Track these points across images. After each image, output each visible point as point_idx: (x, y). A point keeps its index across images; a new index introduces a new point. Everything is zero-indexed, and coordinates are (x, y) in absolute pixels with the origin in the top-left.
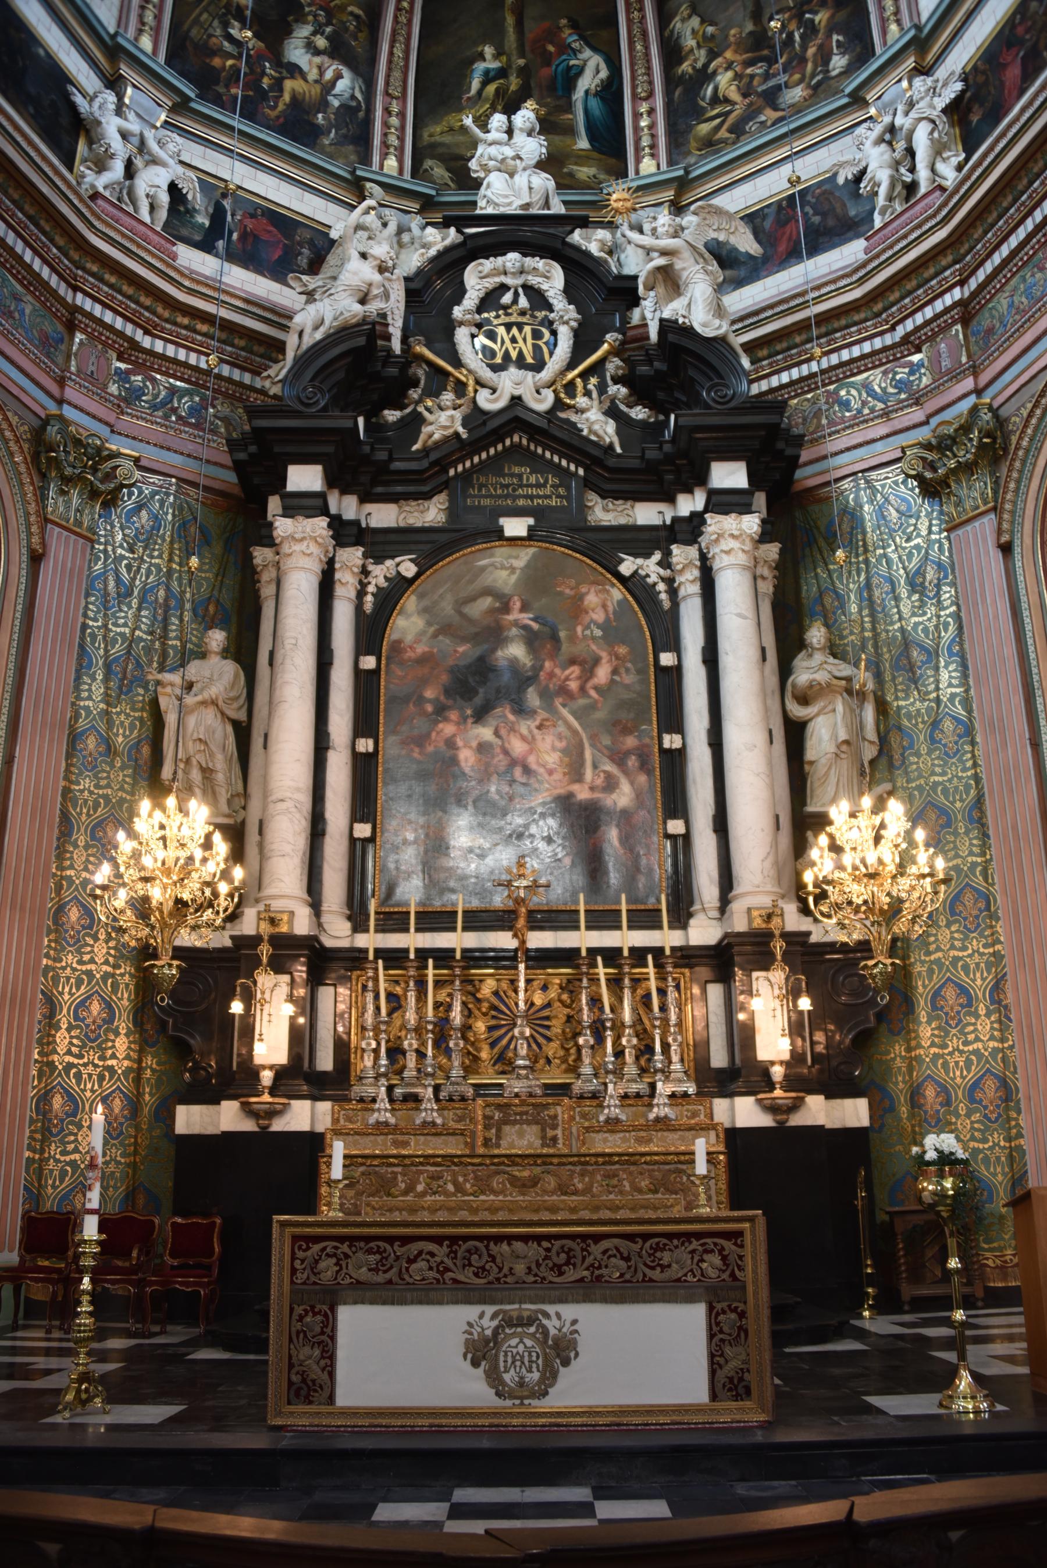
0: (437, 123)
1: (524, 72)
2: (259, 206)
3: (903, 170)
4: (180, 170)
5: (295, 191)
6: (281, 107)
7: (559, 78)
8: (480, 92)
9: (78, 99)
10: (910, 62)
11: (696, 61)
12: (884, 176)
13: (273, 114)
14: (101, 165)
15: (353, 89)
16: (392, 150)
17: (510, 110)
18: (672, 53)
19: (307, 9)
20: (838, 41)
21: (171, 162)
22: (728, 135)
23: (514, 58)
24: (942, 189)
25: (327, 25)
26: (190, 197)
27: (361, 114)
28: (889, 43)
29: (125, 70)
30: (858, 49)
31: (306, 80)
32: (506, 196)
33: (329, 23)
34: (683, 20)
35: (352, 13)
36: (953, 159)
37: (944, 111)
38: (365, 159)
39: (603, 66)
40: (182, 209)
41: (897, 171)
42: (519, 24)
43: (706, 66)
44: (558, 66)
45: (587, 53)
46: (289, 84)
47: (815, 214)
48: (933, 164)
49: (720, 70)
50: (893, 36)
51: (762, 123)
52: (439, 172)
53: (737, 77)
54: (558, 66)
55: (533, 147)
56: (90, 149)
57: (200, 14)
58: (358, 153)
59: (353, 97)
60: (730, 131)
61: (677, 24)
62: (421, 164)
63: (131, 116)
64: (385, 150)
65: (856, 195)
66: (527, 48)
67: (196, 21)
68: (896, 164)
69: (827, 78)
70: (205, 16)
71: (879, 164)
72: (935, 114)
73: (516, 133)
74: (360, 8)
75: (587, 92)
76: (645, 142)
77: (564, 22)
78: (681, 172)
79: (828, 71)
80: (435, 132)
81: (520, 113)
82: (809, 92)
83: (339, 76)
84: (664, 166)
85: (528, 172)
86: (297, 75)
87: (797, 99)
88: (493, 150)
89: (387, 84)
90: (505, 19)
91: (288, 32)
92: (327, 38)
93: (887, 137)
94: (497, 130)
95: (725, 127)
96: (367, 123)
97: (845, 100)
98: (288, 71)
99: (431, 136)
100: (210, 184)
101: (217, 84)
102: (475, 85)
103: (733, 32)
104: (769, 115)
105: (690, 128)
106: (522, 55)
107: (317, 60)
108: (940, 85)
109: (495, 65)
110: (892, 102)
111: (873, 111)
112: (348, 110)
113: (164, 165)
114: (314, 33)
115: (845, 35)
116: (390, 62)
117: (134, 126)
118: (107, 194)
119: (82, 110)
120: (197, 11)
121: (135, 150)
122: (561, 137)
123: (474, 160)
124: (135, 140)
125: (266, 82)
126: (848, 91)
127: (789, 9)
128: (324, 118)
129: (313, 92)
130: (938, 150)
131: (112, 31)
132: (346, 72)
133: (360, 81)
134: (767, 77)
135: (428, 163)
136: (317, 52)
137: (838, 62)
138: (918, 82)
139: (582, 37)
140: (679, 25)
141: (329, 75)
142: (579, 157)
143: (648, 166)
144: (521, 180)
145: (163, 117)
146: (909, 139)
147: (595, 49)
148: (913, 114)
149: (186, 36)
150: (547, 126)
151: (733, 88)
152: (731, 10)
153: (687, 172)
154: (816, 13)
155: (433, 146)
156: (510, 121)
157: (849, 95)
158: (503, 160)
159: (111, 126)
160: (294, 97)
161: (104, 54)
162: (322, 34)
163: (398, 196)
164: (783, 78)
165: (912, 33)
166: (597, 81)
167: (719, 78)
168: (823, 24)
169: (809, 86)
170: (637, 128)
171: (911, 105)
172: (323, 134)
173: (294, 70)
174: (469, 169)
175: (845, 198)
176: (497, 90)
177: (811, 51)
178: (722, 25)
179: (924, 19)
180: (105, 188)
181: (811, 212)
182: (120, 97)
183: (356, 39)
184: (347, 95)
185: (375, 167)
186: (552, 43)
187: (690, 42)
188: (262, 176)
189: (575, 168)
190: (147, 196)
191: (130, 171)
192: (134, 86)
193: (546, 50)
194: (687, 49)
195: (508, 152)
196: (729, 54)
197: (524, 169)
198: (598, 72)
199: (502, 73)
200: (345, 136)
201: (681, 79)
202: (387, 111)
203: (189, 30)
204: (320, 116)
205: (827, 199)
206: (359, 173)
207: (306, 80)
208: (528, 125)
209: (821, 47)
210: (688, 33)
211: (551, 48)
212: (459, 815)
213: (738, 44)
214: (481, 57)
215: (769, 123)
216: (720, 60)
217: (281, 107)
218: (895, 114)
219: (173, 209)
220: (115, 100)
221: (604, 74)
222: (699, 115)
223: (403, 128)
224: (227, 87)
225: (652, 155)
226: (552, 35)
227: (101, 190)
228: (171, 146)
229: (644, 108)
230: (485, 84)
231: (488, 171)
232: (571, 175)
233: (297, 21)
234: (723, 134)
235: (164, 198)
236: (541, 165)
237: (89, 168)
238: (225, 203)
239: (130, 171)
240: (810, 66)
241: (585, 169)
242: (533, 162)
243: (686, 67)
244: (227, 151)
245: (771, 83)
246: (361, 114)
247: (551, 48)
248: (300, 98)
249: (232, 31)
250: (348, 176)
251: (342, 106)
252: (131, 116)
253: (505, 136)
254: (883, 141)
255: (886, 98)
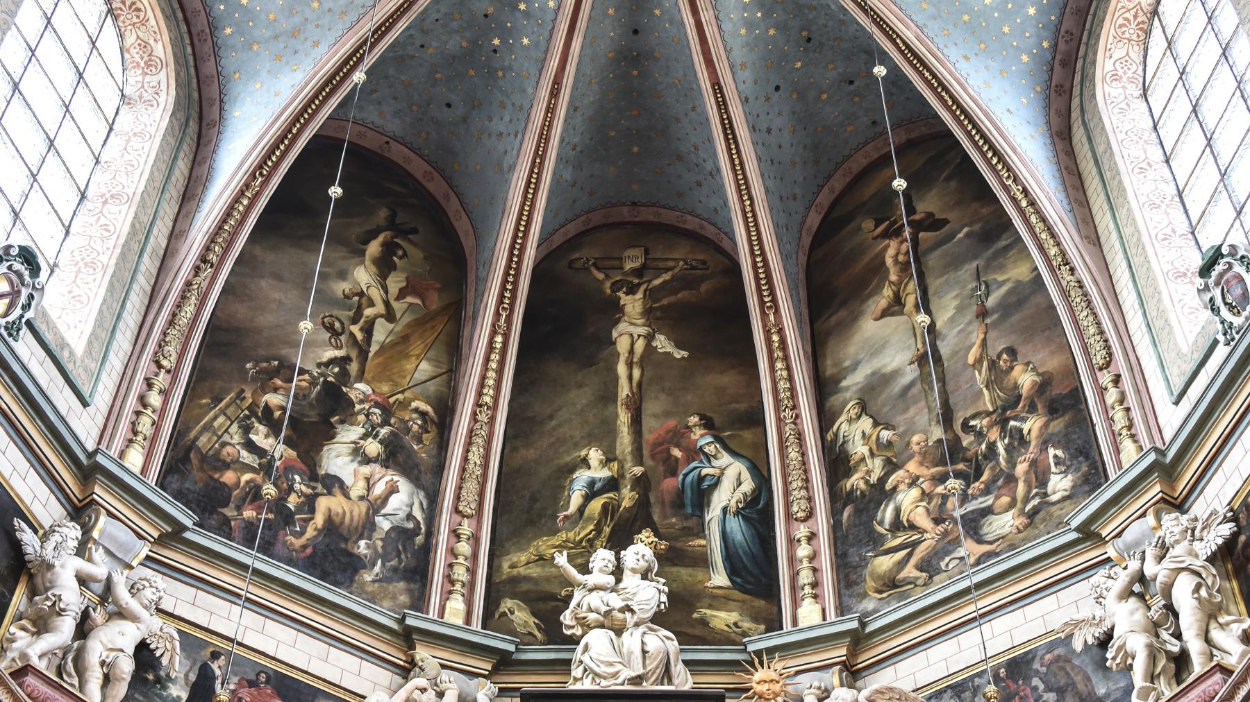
0: (521, 550)
1: (642, 484)
2: (264, 670)
3: (1165, 635)
4: (156, 622)
5: (316, 647)
6: (310, 532)
7: (688, 492)
8: (581, 510)
9: (28, 538)
10: (1155, 490)
11: (868, 472)
12: (1138, 644)
13: (298, 543)
14: (41, 625)
15: (411, 506)
16: (458, 587)
17: (619, 541)
18: (837, 462)
19: (358, 407)
20: (1055, 456)
21: (144, 614)
22: (916, 573)
23: (628, 465)
24: (1227, 672)
25: (382, 426)
26: (165, 661)
27: (419, 539)
28: (1126, 466)
29: (100, 492)
30: (1085, 468)
31: (347, 496)
32: (611, 664)
33: (385, 423)
34: (850, 421)
35: (416, 410)
36: (1234, 626)
37: (1211, 559)
38: (419, 602)
39: (746, 475)
40: (151, 677)
41: (1157, 636)
42: (636, 422)
43: (882, 480)
44: (689, 473)
45: (725, 459)
46: (323, 503)
47: (1049, 689)
48: (1207, 632)
49: (902, 487)
50: (1127, 460)
51: (962, 559)
52: (521, 616)
53: (926, 496)
54: (689, 473)
55: (648, 595)
56: (31, 599)
57: (215, 418)
58: (410, 591)
59: (410, 517)
60: (920, 568)
61: (842, 426)
62: (498, 606)
63: (99, 555)
64: (448, 587)
65: (1101, 664)
66: (646, 453)
67: (208, 427)
68: (1154, 627)
69: (1045, 504)
70: (221, 419)
71: (1128, 623)
72: (1198, 564)
73: (627, 575)
74: (427, 403)
75: (725, 510)
76: (805, 577)
77: (694, 420)
78: (854, 624)
79: (1046, 495)
80: (519, 561)
81: (631, 549)
82: (1024, 520)
83: (393, 490)
84: (832, 615)
85: (642, 629)
86: (336, 490)
87: (1007, 530)
88: (595, 599)
89: (458, 498)
90: (617, 415)
91: (329, 435)
92: (381, 442)
93: (1137, 588)
94: (601, 571)
95: (913, 561)
96: (427, 550)
97: (1073, 536)
98: (324, 486)
99: (513, 566)
100: (195, 640)
101: (227, 505)
102: (576, 500)
103: (916, 438)
104: (969, 549)
105: (864, 562)
106: (639, 461)
107: (366, 470)
108: (1199, 526)
109: (605, 473)
110: (1138, 543)
111: (1111, 552)
112: (402, 534)
113: (134, 619)
114: (365, 436)
115: (1066, 448)
116: (463, 470)
117: (100, 567)
118: (42, 665)
119: (29, 550)
120: (212, 414)
121: (96, 599)
122: (690, 570)
123: (568, 612)
124: (98, 588)
125: (292, 501)
126: (1075, 523)
127: (989, 414)
128: (368, 547)
129: (356, 513)
130: (1211, 613)
131: (90, 447)
132: (404, 485)
133: (422, 494)
134: (964, 499)
135: (507, 604)
136: (367, 460)
137: (1060, 484)
138: (1169, 519)
139: (718, 439)
140: (845, 427)
141: (379, 489)
142: (714, 597)
143: (809, 613)
144: (631, 640)
145: (145, 552)
146: (1167, 591)
147: (734, 453)
148: (1166, 563)
149: (192, 446)
150: (672, 558)
151: (920, 510)
152: (912, 412)
153: (863, 625)
154: (1024, 420)
155: (515, 580)
156: (618, 559)
157: (1077, 529)
158: (607, 614)
159: (67, 569)
160: (329, 520)
161: (75, 476)
162: (375, 437)
163: (462, 653)
164: (989, 501)
165: (1152, 457)
166: (739, 495)
167: (900, 497)
168: (1034, 434)
169: (1022, 513)
170: (792, 559)
171: (1163, 550)
172: (365, 567)
173: (333, 484)
174: (561, 624)
175: (1089, 670)
176: (605, 506)
177: (1021, 469)
178: (901, 429)
179: (1168, 437)
180: (40, 657)
181: (1041, 687)
182: (87, 530)
183: (420, 441)
184: (402, 515)
185: (433, 613)
186: (678, 446)
187: (859, 449)
188: (273, 627)
189: (709, 612)
190: (103, 663)
191: (83, 629)
192: (110, 514)
193: (670, 455)
194: (856, 458)
195: (616, 601)
196: (912, 467)
197: (637, 625)
198: (740, 484)
199: (612, 484)
200: (395, 570)
201: (850, 497)
202: (455, 534)
203: (196, 438)
204: (362, 543)
205: (1063, 669)
206: (410, 621)
207: (347, 496)
208: (643, 564)
209: (1034, 463)
210: (858, 437)
211: (677, 453)
212: (657, 398)
213: (924, 454)
214: (585, 463)
215: (972, 560)
216: (900, 474)
217: (310, 532)
218: (1143, 559)
219: (138, 680)
220: (79, 534)
221: (748, 486)
222: (875, 541)
223: (475, 556)
224: (239, 508)
225: (815, 597)
226: (678, 436)
227: (35, 661)
228: (148, 594)
229: (802, 531)
230: (588, 498)
231: (587, 627)
232: (704, 622)
233: (342, 422)
234: (910, 571)
235: (126, 666)
236: (659, 619)
237: (24, 629)
238: (215, 666)
239: (83, 629)
240: (1021, 489)
241: (722, 614)
242: (650, 614)
243: (855, 481)
244: (231, 595)
245: (972, 506)
246: (419, 539)
247: (677, 453)
248: (337, 520)
249: (253, 437)
250: (395, 626)
251: (393, 529)
252: (99, 555)
253: (612, 579)
254: (1132, 593)
255: (1129, 536)
